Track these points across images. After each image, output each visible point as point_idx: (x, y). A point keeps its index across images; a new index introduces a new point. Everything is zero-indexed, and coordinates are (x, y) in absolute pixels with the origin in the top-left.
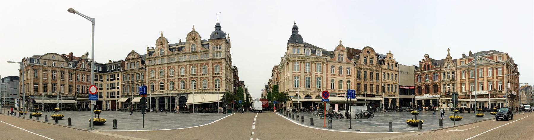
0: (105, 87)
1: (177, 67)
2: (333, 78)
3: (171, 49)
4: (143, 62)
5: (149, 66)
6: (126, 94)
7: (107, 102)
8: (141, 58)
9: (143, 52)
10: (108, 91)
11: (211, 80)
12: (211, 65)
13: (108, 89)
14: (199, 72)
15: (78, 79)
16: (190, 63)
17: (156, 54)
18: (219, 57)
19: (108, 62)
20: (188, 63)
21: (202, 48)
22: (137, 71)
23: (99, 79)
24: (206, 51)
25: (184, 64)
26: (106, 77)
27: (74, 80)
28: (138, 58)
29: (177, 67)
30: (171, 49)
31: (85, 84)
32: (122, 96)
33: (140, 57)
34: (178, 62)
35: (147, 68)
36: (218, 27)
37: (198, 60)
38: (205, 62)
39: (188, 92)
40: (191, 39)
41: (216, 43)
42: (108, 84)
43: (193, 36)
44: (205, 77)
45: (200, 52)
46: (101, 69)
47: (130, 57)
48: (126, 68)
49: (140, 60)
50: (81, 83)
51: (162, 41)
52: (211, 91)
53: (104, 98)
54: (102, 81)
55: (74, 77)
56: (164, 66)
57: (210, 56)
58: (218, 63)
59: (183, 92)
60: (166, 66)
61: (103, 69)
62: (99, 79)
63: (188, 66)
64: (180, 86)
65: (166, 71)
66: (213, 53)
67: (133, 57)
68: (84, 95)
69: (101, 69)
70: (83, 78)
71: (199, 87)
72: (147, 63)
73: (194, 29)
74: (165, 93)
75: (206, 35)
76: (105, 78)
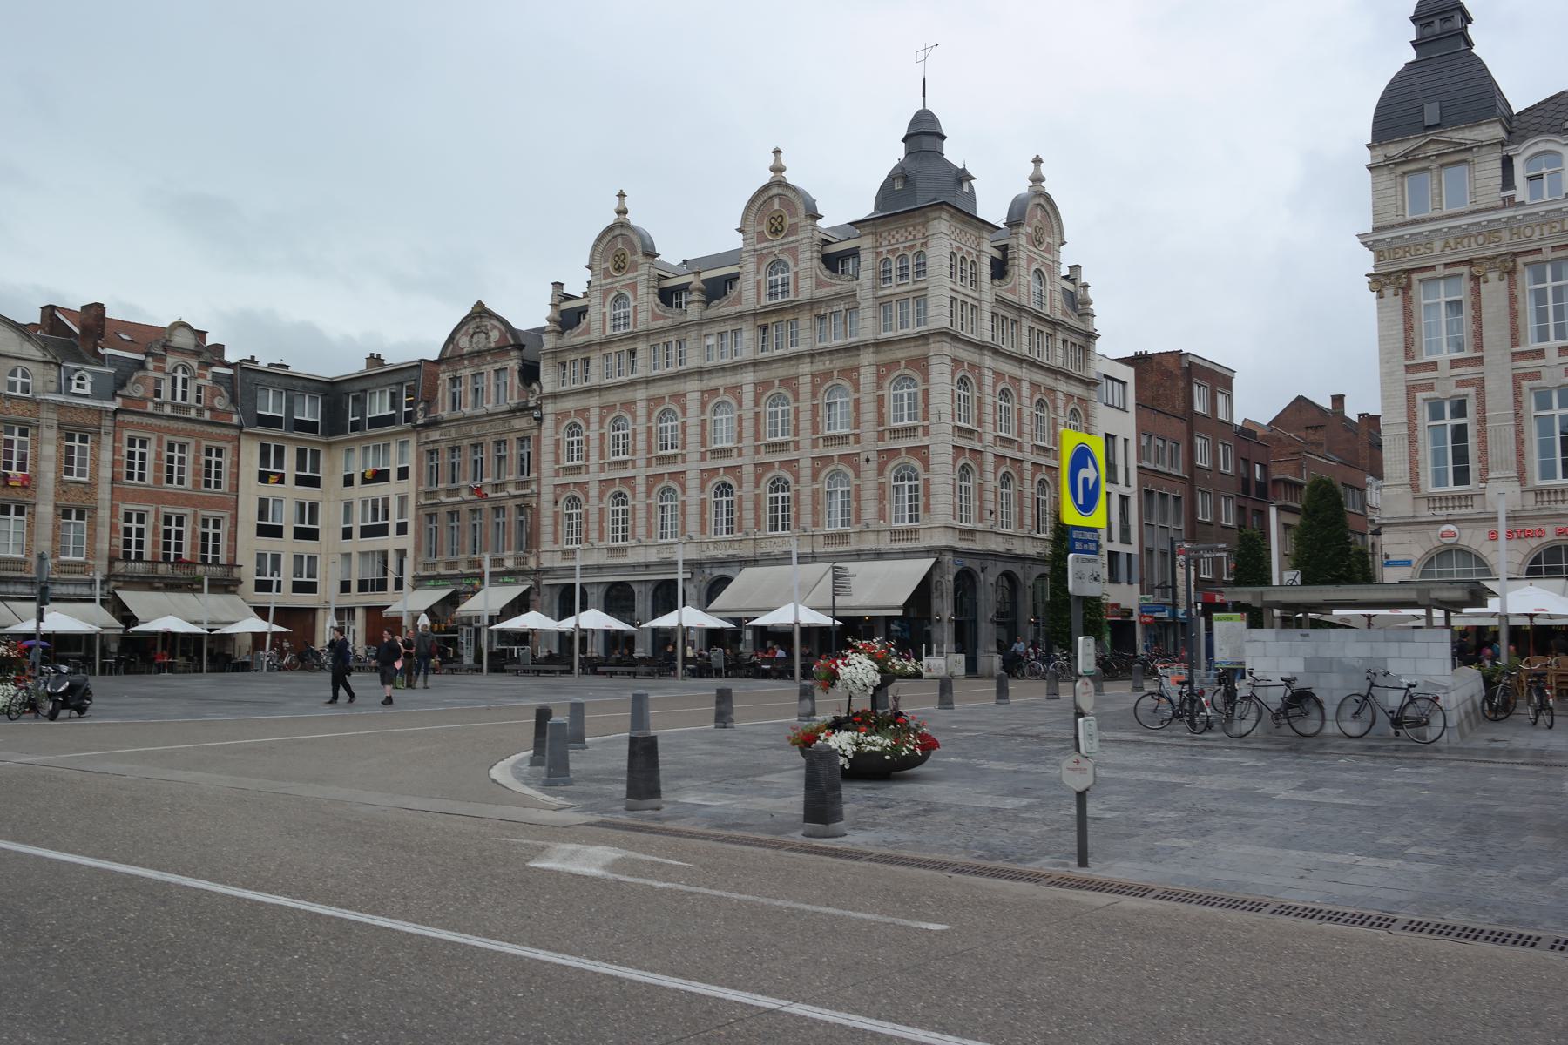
0: (329, 521)
1: (693, 400)
2: (271, 490)
3: (668, 295)
4: (530, 373)
5: (554, 396)
6: (442, 570)
7: (344, 613)
8: (520, 347)
9: (528, 312)
10: (348, 546)
11: (870, 471)
12: (867, 377)
13: (347, 534)
14: (805, 425)
15: (132, 466)
16: (763, 375)
17: (597, 324)
18: (913, 329)
19: (358, 366)
20: (748, 377)
21: (825, 275)
22: (499, 427)
23: (290, 467)
24: (839, 297)
25: (730, 380)
26: (339, 454)
27: (106, 473)
28: (502, 350)
29: (693, 400)
30: (668, 295)
31: (188, 501)
32: (420, 582)
33: (514, 341)
34: (700, 373)
35: (548, 408)
36: (924, 135)
37: (799, 357)
38: (839, 363)
39: (747, 551)
40: (764, 228)
41: (899, 239)
42: (348, 506)
43: (777, 207)
44: (839, 460)
45: (811, 304)
46: (309, 411)
47: (464, 343)
48: (444, 411)
49: (513, 363)
50: (158, 499)
51: (620, 246)
52: (870, 543)
53: (328, 593)
54: (314, 482)
55: (106, 456)
56: (628, 395)
57: (867, 327)
58: (911, 362)
59: (721, 553)
60: (641, 394)
61: (336, 407)
62: (290, 467)
63: (748, 393)
64: (608, 525)
65: (641, 429)
66: (883, 304)
67: (483, 337)
68: (140, 568)
69: (309, 411)
70: (169, 471)
71: (806, 518)
72: (548, 380)
73: (778, 169)
74: (633, 557)
75: (845, 192)
76: (332, 466)
